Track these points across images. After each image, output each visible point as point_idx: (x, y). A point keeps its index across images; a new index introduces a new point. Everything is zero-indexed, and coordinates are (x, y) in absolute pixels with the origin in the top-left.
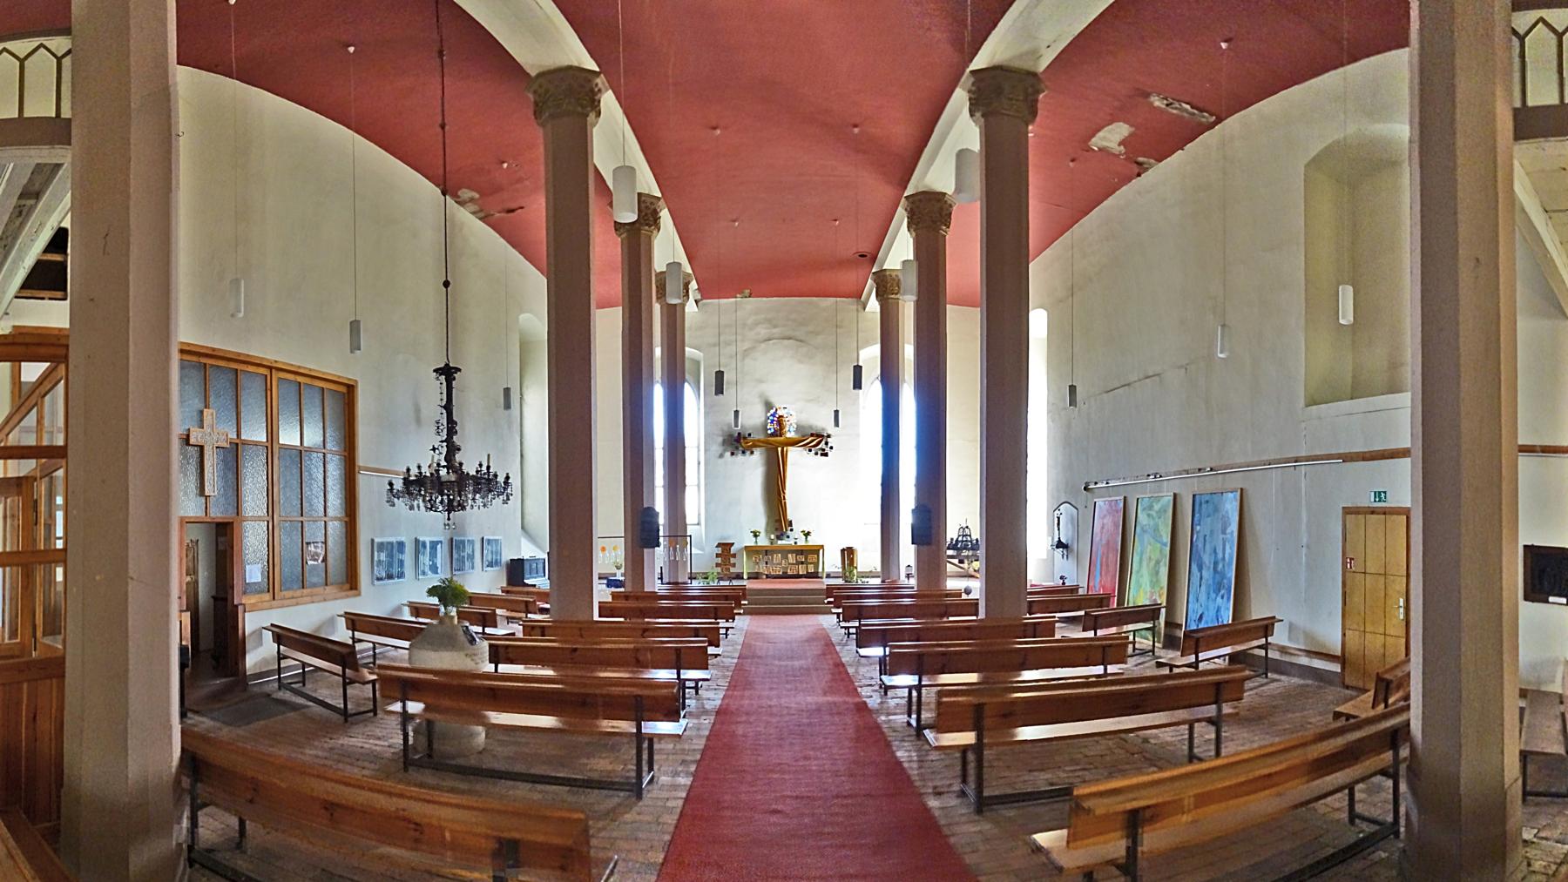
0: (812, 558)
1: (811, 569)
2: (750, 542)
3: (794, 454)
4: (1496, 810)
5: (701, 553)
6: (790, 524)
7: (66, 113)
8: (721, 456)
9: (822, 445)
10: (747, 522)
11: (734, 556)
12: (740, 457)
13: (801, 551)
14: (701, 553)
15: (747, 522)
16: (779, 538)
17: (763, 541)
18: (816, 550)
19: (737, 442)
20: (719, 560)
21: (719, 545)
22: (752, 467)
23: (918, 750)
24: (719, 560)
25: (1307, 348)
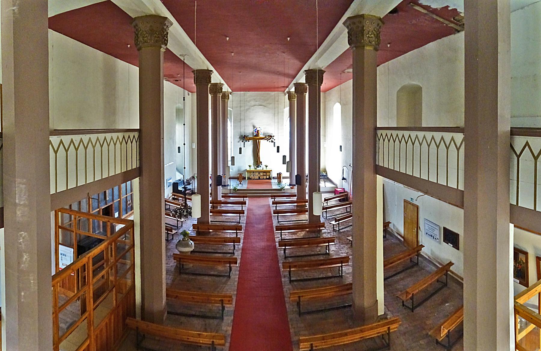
6: (261, 163)
19: (244, 138)
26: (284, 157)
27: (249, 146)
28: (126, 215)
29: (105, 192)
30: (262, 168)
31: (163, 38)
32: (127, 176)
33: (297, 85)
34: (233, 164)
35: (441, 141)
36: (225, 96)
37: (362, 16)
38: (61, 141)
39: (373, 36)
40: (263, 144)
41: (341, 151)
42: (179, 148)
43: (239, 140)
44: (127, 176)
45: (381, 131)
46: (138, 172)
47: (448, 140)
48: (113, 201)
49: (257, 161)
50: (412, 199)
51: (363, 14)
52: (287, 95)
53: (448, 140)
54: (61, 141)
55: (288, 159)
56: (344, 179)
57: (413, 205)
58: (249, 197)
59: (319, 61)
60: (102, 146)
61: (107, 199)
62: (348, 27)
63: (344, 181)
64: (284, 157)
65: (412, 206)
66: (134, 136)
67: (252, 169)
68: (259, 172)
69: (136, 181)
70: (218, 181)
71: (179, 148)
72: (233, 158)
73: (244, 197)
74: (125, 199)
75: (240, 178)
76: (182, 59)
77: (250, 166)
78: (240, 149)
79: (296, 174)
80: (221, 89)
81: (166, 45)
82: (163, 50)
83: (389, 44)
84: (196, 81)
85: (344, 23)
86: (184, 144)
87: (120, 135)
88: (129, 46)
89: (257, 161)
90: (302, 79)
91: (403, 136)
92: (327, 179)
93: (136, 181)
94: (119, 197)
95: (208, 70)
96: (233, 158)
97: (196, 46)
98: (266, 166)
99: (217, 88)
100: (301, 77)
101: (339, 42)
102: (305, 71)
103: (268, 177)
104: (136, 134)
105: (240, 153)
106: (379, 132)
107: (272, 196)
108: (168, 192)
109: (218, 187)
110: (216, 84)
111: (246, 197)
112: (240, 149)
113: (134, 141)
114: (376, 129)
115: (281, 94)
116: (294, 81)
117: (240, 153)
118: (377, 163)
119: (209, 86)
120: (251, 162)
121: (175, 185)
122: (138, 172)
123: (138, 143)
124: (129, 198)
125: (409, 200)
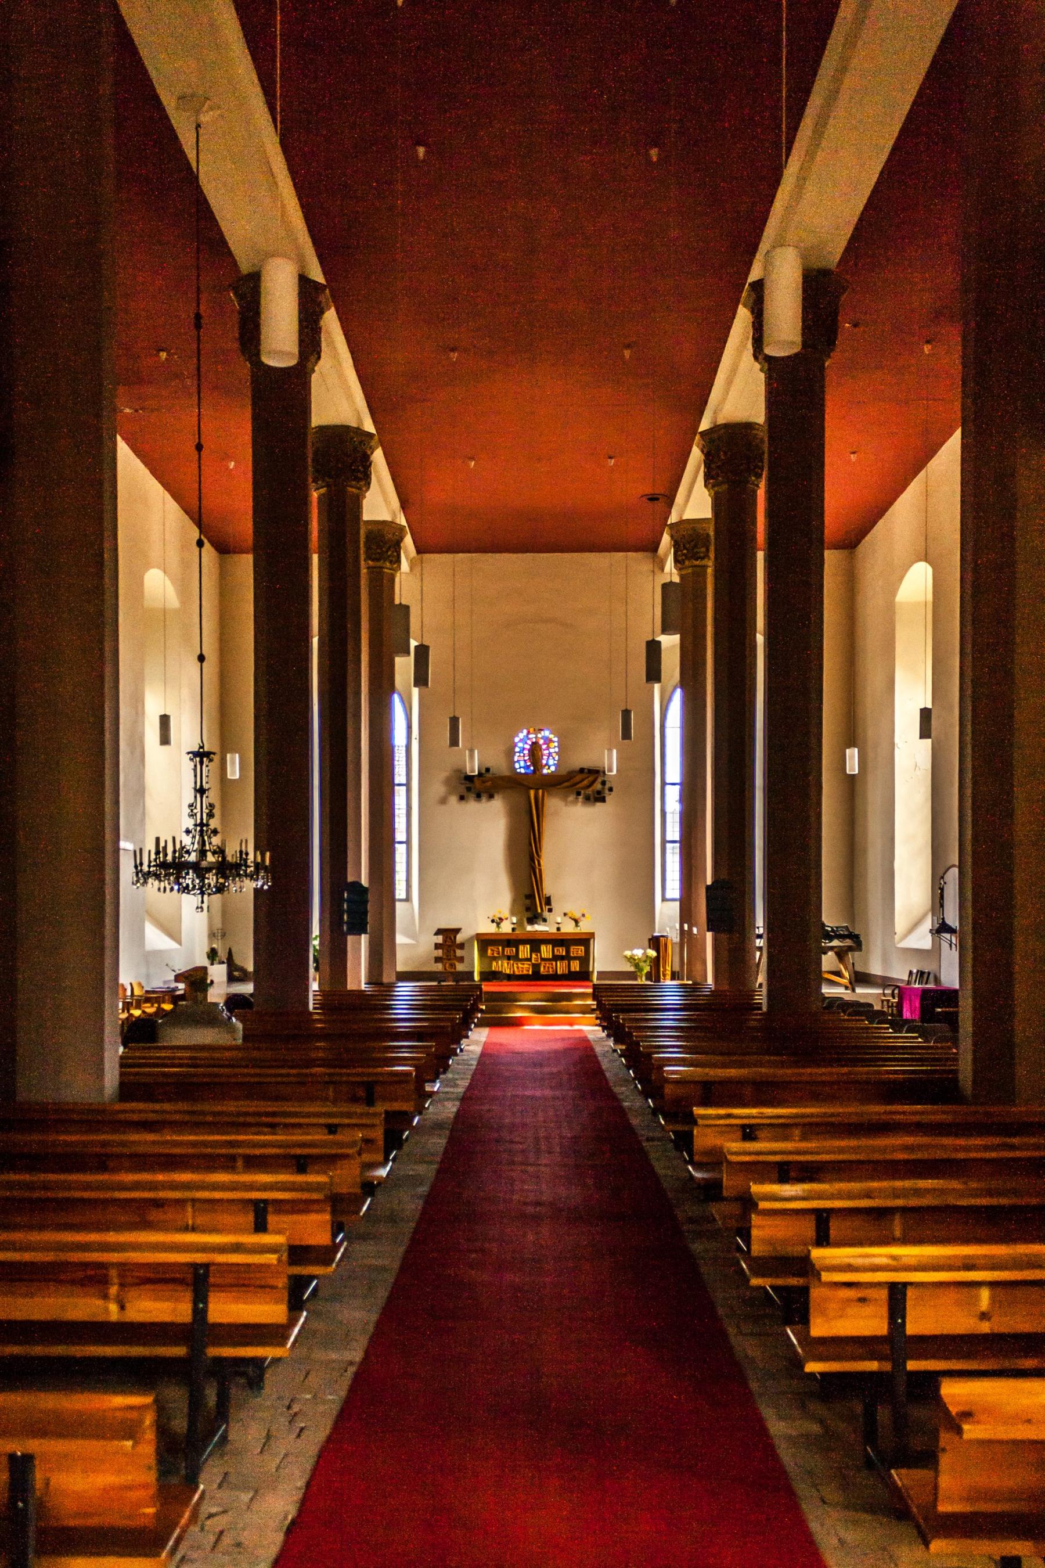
0: (578, 951)
1: (575, 966)
2: (488, 928)
3: (553, 804)
4: (226, 878)
5: (412, 942)
6: (548, 901)
7: (590, 990)
8: (443, 801)
9: (598, 786)
10: (485, 907)
11: (462, 946)
12: (472, 806)
13: (560, 941)
14: (412, 942)
15: (485, 907)
16: (531, 921)
17: (506, 928)
18: (585, 941)
19: (475, 786)
20: (440, 953)
21: (439, 932)
22: (490, 824)
23: (829, 1409)
24: (440, 953)
25: (233, 1200)
49: (531, 900)
68: (535, 943)
89: (531, 900)
116: (376, 437)
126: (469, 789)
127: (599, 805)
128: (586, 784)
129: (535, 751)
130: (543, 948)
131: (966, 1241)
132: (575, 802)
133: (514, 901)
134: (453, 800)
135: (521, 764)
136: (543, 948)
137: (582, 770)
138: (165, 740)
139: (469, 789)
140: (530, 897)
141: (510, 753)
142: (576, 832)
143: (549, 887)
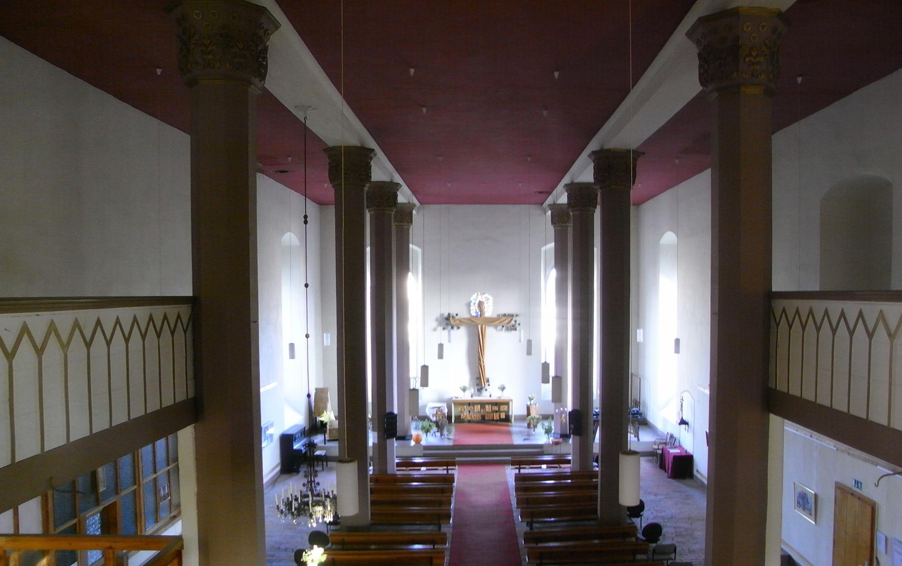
3: (490, 331)
6: (488, 381)
9: (513, 322)
19: (448, 321)
26: (546, 366)
27: (459, 339)
28: (156, 527)
29: (94, 474)
30: (492, 393)
31: (256, 62)
32: (162, 423)
33: (574, 190)
34: (425, 383)
35: (823, 319)
36: (405, 215)
37: (735, 13)
38: (52, 323)
39: (761, 59)
40: (494, 338)
41: (677, 351)
42: (292, 346)
43: (435, 324)
44: (162, 423)
45: (785, 303)
46: (191, 411)
47: (852, 317)
48: (117, 491)
49: (479, 381)
50: (857, 482)
51: (738, 8)
52: (549, 213)
53: (852, 317)
54: (52, 323)
55: (552, 373)
56: (683, 422)
57: (862, 499)
58: (462, 464)
59: (635, 123)
60: (127, 340)
61: (102, 489)
62: (698, 43)
63: (683, 426)
64: (546, 366)
65: (857, 503)
66: (179, 317)
67: (467, 396)
68: (483, 404)
69: (186, 437)
70: (390, 427)
71: (292, 346)
72: (425, 369)
73: (447, 464)
74: (151, 484)
75: (442, 423)
76: (300, 115)
77: (464, 390)
78: (441, 346)
79: (569, 408)
80: (395, 196)
81: (263, 77)
82: (254, 91)
83: (801, 75)
84: (334, 175)
85: (689, 34)
86: (307, 336)
87: (142, 313)
88: (159, 71)
89: (479, 381)
90: (584, 171)
91: (797, 312)
92: (643, 423)
93: (186, 437)
94: (135, 480)
95: (392, 183)
96: (425, 369)
97: (345, 98)
98: (503, 389)
99: (388, 192)
100: (561, 194)
101: (670, 84)
102: (594, 153)
103: (503, 416)
104: (185, 311)
105: (441, 356)
106: (778, 305)
107: (513, 463)
108: (270, 457)
109: (388, 441)
110: (381, 185)
111: (454, 464)
112: (441, 346)
113: (136, 336)
114: (771, 296)
115: (534, 209)
116: (566, 180)
117: (441, 356)
118: (772, 385)
119: (366, 189)
120: (465, 377)
121: (286, 440)
122: (191, 411)
123: (189, 332)
124: (163, 482)
125: (850, 484)
126: (447, 324)
127: (513, 332)
128: (508, 322)
129: (480, 304)
130: (487, 406)
131: (391, 274)
132: (501, 330)
133: (471, 379)
134: (440, 329)
135: (474, 310)
136: (487, 406)
137: (505, 315)
138: (292, 356)
139: (447, 324)
140: (479, 378)
141: (469, 305)
142: (498, 343)
143: (488, 373)
